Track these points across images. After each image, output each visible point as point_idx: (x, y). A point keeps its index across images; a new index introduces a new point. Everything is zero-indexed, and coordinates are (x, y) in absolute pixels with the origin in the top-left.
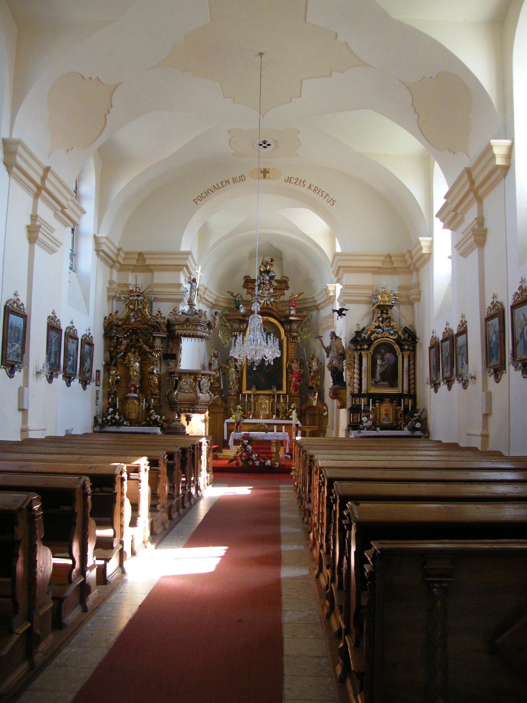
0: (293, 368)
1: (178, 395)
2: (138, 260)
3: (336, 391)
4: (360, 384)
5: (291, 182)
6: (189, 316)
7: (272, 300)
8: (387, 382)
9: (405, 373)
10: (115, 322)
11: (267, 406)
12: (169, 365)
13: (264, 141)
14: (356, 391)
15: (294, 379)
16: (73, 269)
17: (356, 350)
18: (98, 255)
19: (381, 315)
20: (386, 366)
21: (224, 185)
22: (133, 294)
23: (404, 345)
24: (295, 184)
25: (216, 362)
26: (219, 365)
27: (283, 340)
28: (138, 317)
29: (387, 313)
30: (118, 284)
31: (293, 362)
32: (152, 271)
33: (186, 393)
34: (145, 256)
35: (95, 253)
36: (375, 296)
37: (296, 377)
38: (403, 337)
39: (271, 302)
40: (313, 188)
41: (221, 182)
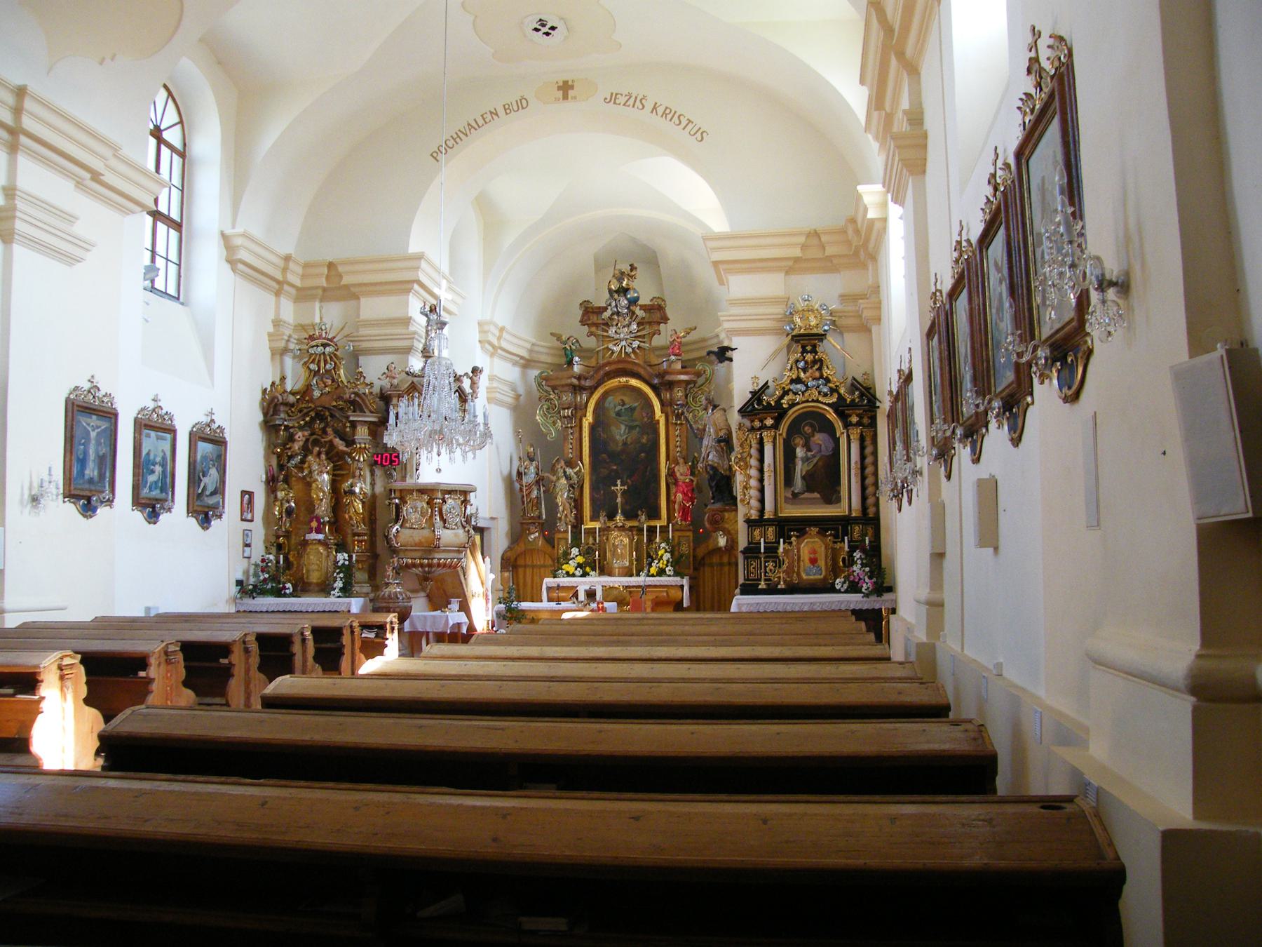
1: (400, 534)
2: (328, 278)
3: (713, 516)
4: (762, 501)
5: (618, 101)
6: (415, 380)
7: (636, 344)
8: (818, 492)
9: (853, 472)
10: (280, 397)
12: (391, 476)
13: (540, 20)
14: (754, 515)
15: (680, 496)
16: (181, 300)
17: (752, 429)
18: (234, 270)
19: (802, 355)
20: (815, 460)
21: (487, 120)
22: (314, 343)
23: (850, 416)
24: (624, 105)
25: (532, 469)
26: (537, 474)
27: (658, 421)
28: (326, 386)
29: (814, 351)
30: (295, 326)
31: (678, 464)
32: (356, 297)
34: (340, 269)
35: (227, 267)
36: (789, 317)
37: (683, 493)
38: (849, 400)
39: (633, 349)
40: (660, 110)
41: (482, 116)
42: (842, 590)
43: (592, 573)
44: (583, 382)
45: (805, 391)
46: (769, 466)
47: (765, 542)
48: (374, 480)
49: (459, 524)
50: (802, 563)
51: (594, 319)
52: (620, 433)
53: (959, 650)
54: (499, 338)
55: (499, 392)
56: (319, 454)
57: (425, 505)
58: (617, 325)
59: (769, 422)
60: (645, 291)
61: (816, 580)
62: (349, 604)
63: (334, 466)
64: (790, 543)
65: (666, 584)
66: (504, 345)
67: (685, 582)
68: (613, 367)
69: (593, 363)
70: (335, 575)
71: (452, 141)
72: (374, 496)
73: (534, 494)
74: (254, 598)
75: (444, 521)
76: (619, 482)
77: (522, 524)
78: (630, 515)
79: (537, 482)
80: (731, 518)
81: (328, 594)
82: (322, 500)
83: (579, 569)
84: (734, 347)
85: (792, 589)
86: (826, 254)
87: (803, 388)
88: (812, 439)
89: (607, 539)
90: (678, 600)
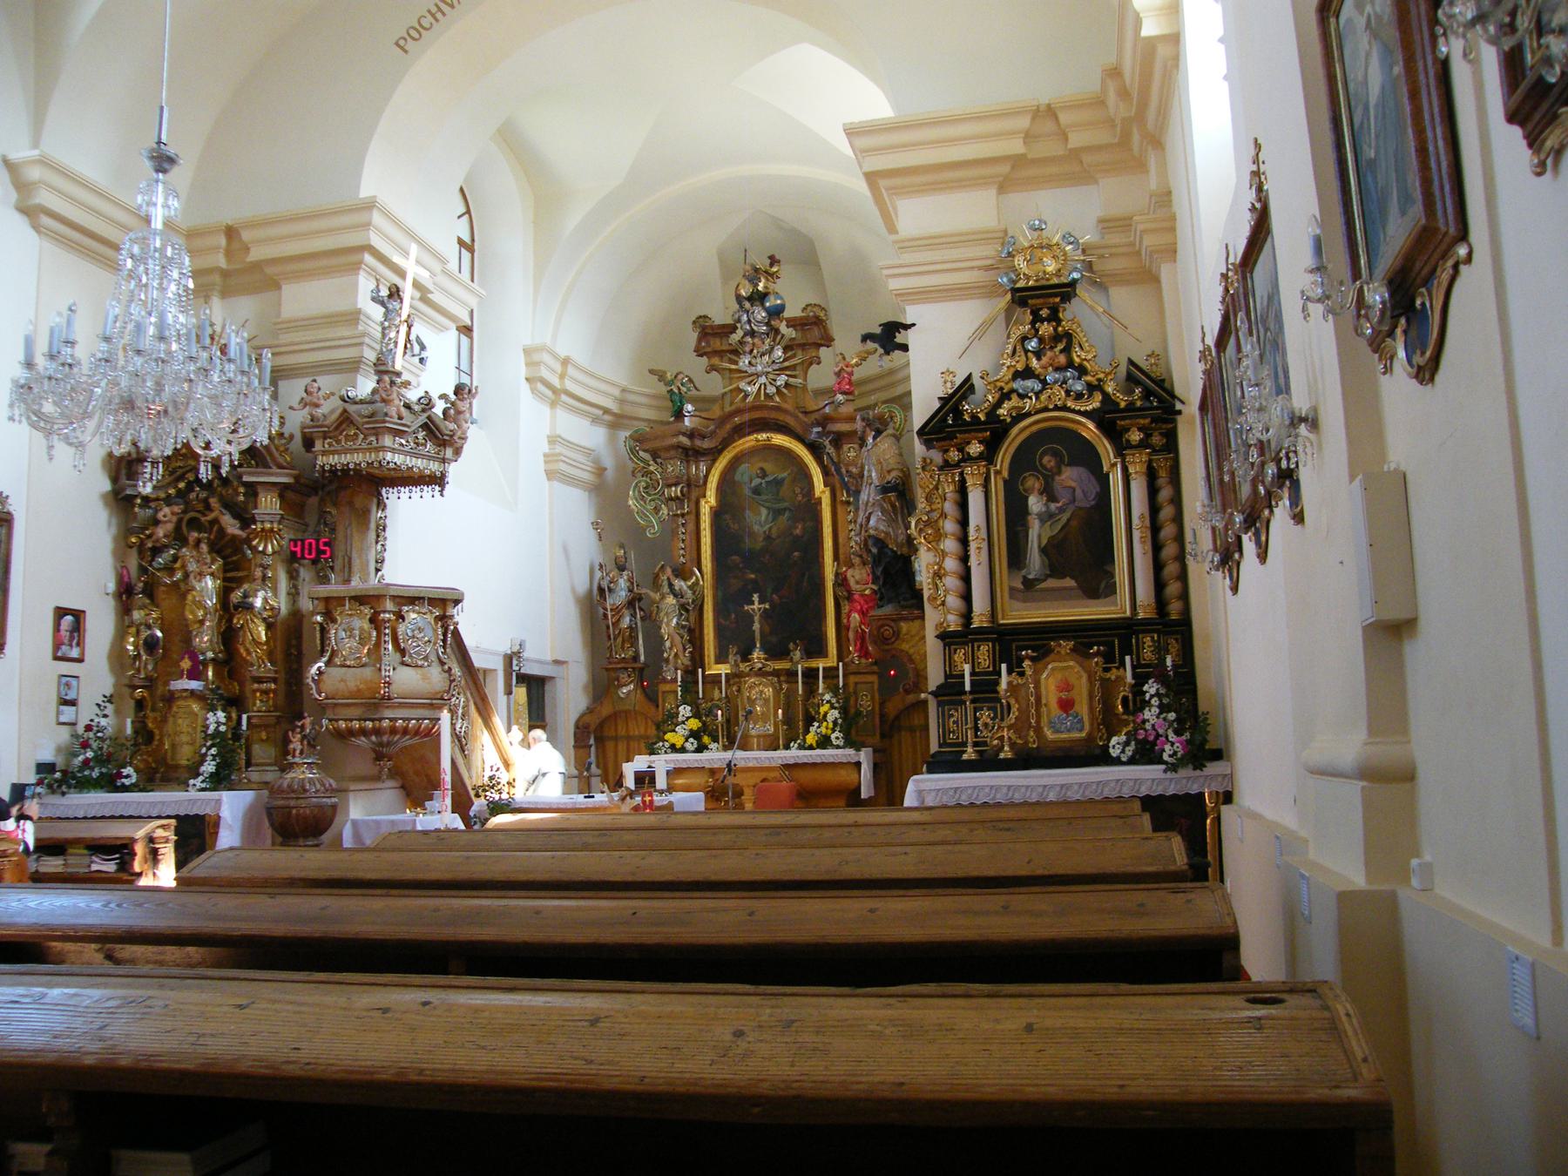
0: (852, 582)
1: (324, 677)
2: (229, 254)
4: (967, 597)
8: (1072, 578)
9: (1136, 535)
11: (768, 710)
15: (856, 616)
17: (946, 466)
18: (36, 227)
20: (1065, 517)
23: (1128, 430)
25: (622, 583)
26: (630, 591)
29: (1054, 317)
31: (851, 565)
32: (274, 285)
33: (349, 667)
34: (246, 235)
42: (1124, 759)
43: (713, 746)
44: (698, 443)
45: (1041, 391)
46: (978, 529)
47: (973, 674)
48: (295, 587)
49: (433, 658)
50: (1044, 709)
51: (717, 344)
52: (759, 521)
53: (1544, 940)
54: (562, 377)
55: (564, 462)
56: (198, 542)
57: (366, 625)
58: (752, 351)
59: (975, 448)
60: (793, 296)
61: (1072, 741)
62: (219, 802)
63: (225, 564)
64: (1022, 674)
65: (832, 760)
66: (570, 386)
67: (865, 757)
68: (746, 417)
69: (716, 412)
70: (204, 750)
71: (429, 17)
72: (297, 616)
73: (626, 622)
74: (63, 794)
75: (403, 652)
76: (756, 597)
77: (607, 670)
78: (777, 651)
79: (631, 604)
80: (913, 633)
81: (184, 785)
82: (202, 622)
83: (691, 740)
84: (909, 322)
85: (1026, 760)
86: (1069, 146)
87: (1038, 387)
88: (1057, 478)
89: (739, 691)
90: (852, 787)
